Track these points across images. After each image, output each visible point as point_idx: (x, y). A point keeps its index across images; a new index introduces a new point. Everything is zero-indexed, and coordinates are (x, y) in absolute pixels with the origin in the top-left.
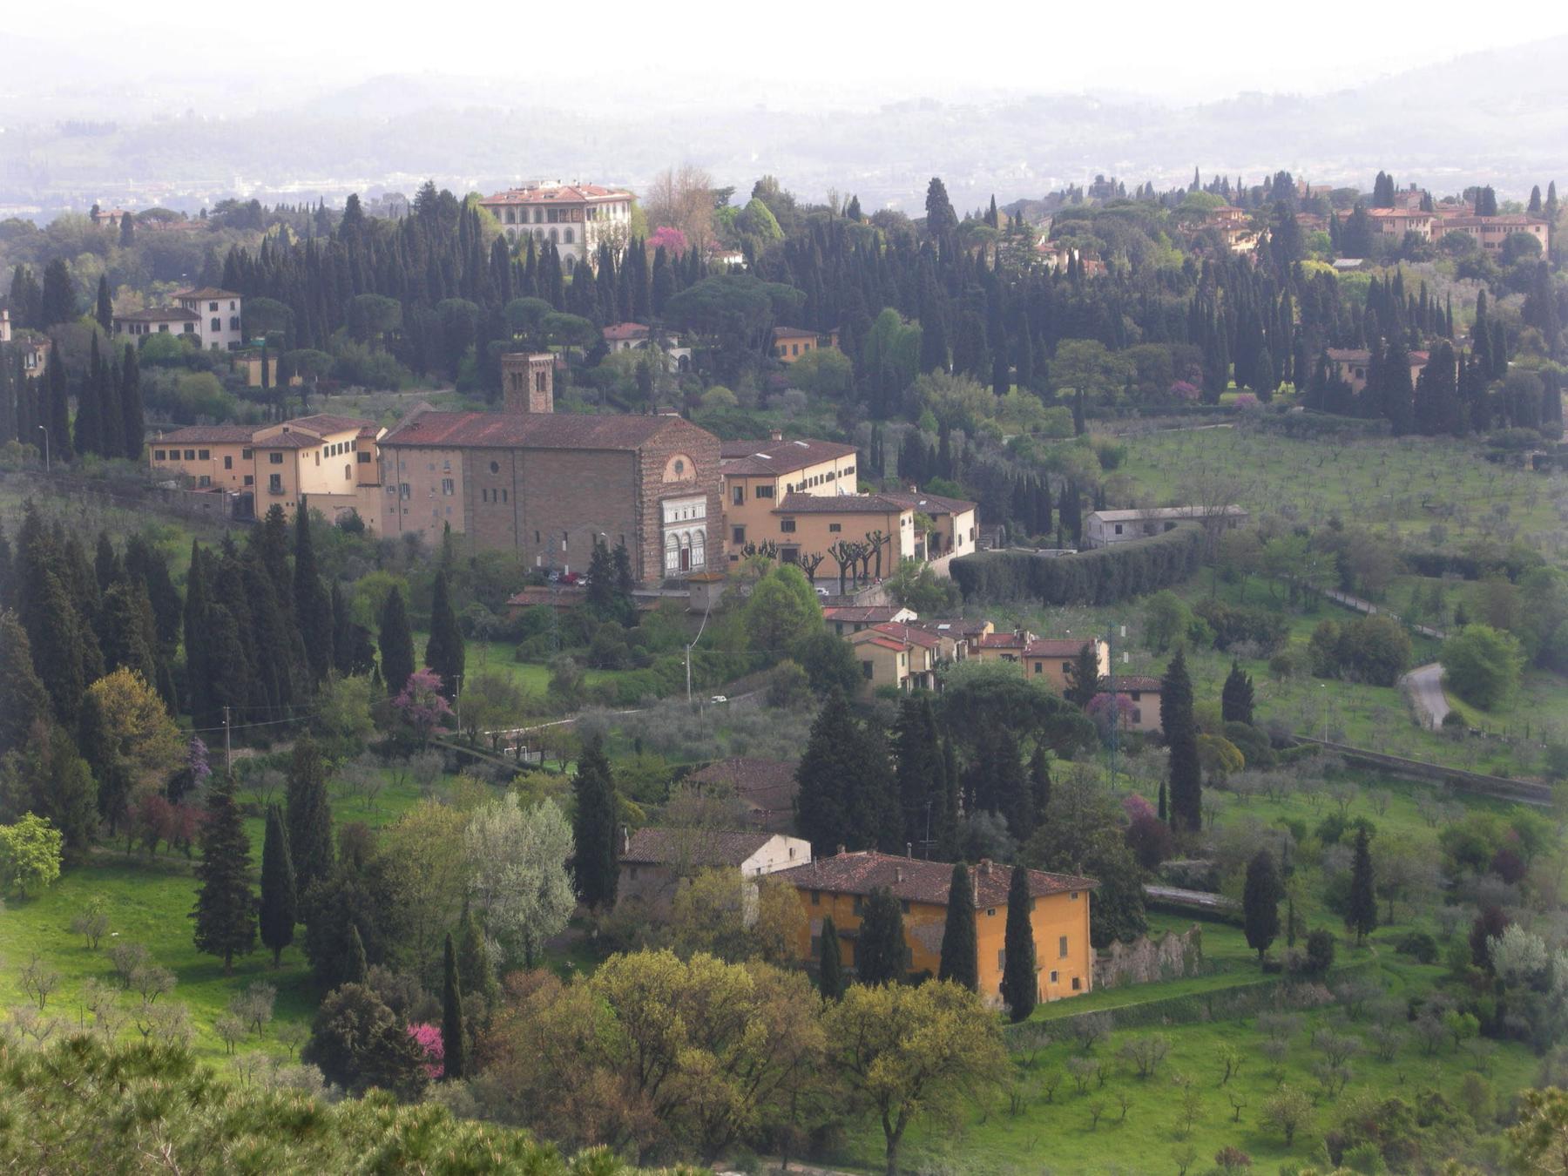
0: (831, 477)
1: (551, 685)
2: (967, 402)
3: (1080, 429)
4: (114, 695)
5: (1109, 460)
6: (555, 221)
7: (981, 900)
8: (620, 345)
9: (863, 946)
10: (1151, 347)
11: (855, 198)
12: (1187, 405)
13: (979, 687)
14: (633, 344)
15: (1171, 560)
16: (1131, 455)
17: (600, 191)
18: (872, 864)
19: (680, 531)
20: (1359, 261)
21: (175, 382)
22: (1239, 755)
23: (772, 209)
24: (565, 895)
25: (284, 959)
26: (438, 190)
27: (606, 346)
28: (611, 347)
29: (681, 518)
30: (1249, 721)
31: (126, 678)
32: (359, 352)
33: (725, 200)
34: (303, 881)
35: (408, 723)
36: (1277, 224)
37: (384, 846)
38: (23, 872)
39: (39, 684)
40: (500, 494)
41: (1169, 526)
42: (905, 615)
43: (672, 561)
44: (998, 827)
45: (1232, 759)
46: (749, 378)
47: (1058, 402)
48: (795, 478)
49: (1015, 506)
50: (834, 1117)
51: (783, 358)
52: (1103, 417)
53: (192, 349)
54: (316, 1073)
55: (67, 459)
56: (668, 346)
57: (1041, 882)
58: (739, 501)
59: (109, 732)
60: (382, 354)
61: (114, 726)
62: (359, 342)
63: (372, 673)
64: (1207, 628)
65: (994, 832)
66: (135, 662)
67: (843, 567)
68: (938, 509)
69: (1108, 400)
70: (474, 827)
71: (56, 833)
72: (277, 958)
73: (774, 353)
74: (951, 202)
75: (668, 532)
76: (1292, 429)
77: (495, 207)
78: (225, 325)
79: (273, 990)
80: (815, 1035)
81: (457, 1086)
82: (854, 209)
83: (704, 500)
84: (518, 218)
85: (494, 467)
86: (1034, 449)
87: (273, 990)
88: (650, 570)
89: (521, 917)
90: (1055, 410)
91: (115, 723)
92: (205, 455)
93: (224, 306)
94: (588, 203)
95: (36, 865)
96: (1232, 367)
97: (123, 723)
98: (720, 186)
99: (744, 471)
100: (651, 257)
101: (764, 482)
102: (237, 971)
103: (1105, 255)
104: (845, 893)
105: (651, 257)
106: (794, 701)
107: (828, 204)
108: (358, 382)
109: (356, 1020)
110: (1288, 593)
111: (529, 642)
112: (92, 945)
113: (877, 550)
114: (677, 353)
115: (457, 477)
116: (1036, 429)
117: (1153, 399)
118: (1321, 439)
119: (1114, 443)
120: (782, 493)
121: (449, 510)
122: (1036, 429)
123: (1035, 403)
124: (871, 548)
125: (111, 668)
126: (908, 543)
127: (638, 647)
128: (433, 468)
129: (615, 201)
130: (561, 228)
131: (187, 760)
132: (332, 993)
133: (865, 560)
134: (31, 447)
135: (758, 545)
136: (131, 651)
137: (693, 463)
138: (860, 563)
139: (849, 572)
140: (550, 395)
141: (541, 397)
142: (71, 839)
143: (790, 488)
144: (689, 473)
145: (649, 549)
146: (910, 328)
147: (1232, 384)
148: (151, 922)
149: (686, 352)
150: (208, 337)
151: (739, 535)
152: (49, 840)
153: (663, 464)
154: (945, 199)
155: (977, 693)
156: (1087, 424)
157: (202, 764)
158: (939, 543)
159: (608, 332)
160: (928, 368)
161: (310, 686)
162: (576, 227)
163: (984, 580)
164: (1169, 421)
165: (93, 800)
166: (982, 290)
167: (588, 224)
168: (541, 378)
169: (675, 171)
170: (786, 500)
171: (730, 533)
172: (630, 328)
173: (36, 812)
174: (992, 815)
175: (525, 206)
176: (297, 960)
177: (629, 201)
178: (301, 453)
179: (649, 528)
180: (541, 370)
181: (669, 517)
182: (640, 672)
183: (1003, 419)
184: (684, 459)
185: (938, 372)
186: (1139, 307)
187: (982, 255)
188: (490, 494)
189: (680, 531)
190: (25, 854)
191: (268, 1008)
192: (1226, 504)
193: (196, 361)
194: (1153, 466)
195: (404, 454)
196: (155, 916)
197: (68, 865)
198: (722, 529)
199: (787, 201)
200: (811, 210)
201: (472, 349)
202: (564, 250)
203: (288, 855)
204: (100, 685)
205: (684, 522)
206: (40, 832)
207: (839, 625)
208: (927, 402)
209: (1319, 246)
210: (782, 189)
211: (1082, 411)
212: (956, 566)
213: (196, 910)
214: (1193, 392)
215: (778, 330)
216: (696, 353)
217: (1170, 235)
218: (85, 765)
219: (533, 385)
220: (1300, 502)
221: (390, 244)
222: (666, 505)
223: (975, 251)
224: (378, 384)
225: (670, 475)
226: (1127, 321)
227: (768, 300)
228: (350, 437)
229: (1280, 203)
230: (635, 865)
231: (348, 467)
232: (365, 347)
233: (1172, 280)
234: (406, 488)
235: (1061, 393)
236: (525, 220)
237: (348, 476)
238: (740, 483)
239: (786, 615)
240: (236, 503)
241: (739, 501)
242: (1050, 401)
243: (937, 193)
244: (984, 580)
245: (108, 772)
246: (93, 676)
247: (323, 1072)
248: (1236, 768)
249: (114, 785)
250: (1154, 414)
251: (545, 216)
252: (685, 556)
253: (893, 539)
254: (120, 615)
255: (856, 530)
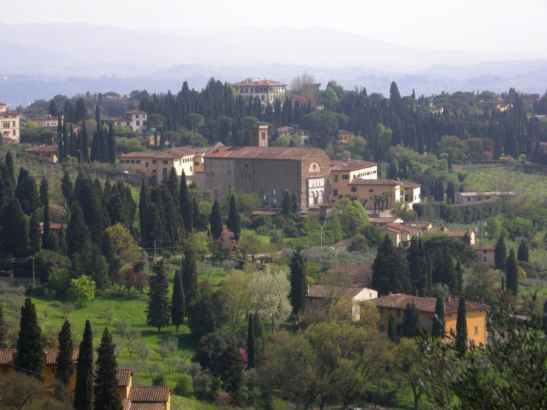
0: (368, 174)
1: (271, 240)
2: (409, 157)
3: (450, 167)
4: (115, 232)
5: (461, 178)
6: (258, 92)
7: (446, 311)
8: (283, 135)
9: (402, 325)
10: (475, 139)
11: (365, 88)
12: (488, 160)
13: (436, 240)
15: (490, 209)
16: (469, 177)
17: (274, 82)
18: (403, 298)
19: (314, 190)
20: (544, 116)
21: (124, 141)
22: (525, 273)
23: (335, 91)
24: (288, 307)
25: (179, 329)
26: (216, 80)
29: (315, 186)
30: (527, 261)
31: (119, 226)
33: (318, 88)
34: (188, 300)
35: (220, 250)
36: (515, 102)
38: (81, 296)
39: (87, 228)
40: (248, 176)
41: (488, 197)
42: (399, 221)
43: (311, 201)
44: (445, 289)
45: (522, 275)
46: (330, 146)
47: (442, 158)
48: (356, 173)
49: (432, 189)
50: (393, 389)
51: (341, 141)
52: (458, 163)
53: (129, 131)
54: (198, 365)
55: (88, 163)
56: (300, 135)
57: (468, 305)
58: (336, 180)
59: (112, 246)
61: (115, 244)
64: (506, 231)
65: (443, 291)
66: (122, 221)
67: (375, 204)
68: (408, 186)
69: (460, 158)
70: (254, 280)
71: (93, 282)
72: (177, 329)
73: (338, 139)
74: (399, 90)
75: (310, 190)
76: (527, 170)
77: (236, 86)
78: (141, 123)
79: (177, 339)
80: (390, 355)
81: (253, 370)
82: (364, 91)
83: (323, 179)
84: (244, 91)
85: (246, 166)
86: (434, 173)
87: (177, 339)
88: (303, 204)
89: (271, 314)
90: (441, 161)
91: (115, 243)
92: (138, 162)
93: (141, 116)
94: (270, 86)
95: (86, 294)
96: (503, 149)
97: (118, 243)
98: (317, 83)
99: (338, 169)
100: (293, 104)
101: (345, 174)
102: (163, 333)
103: (454, 110)
104: (394, 308)
105: (293, 104)
106: (361, 249)
107: (354, 90)
108: (191, 144)
109: (213, 346)
110: (531, 223)
111: (260, 228)
112: (107, 323)
113: (386, 199)
114: (304, 137)
115: (232, 169)
116: (434, 167)
117: (475, 157)
118: (538, 172)
119: (463, 172)
120: (351, 178)
121: (229, 182)
122: (434, 167)
123: (433, 157)
124: (385, 198)
125: (113, 223)
126: (398, 196)
128: (223, 166)
129: (279, 86)
130: (260, 95)
131: (140, 259)
132: (204, 337)
133: (383, 202)
134: (75, 158)
135: (344, 195)
136: (120, 218)
138: (381, 203)
139: (377, 205)
140: (267, 141)
141: (263, 141)
142: (99, 286)
143: (354, 176)
144: (318, 169)
145: (303, 196)
146: (387, 131)
147: (503, 154)
148: (129, 316)
150: (135, 128)
151: (335, 193)
152: (90, 285)
153: (309, 165)
154: (397, 89)
155: (435, 241)
156: (453, 166)
157: (146, 260)
158: (409, 198)
159: (279, 129)
160: (394, 145)
162: (265, 95)
163: (425, 211)
164: (482, 166)
165: (107, 270)
166: (412, 119)
167: (270, 94)
169: (301, 77)
170: (353, 180)
171: (332, 192)
172: (286, 128)
173: (85, 274)
174: (443, 285)
175: (247, 87)
176: (185, 329)
177: (284, 86)
179: (303, 189)
180: (263, 131)
181: (310, 185)
183: (424, 162)
184: (316, 164)
185: (398, 146)
186: (469, 126)
187: (412, 108)
189: (314, 190)
190: (81, 289)
191: (176, 345)
192: (508, 191)
193: (130, 135)
194: (477, 181)
195: (213, 161)
196: (130, 314)
197: (96, 295)
198: (330, 191)
199: (340, 88)
200: (348, 92)
201: (231, 133)
202: (263, 103)
203: (182, 289)
204: (109, 229)
205: (316, 187)
206: (87, 281)
207: (375, 224)
208: (395, 156)
209: (530, 111)
210: (338, 84)
211: (451, 162)
212: (415, 206)
213: (148, 310)
214: (490, 154)
215: (340, 131)
216: (310, 139)
217: (477, 104)
218: (103, 258)
219: (260, 136)
220: (532, 194)
221: (200, 97)
222: (310, 181)
223: (409, 107)
224: (197, 145)
225: (311, 170)
226: (466, 131)
227: (337, 119)
228: (192, 156)
229: (513, 97)
230: (311, 298)
231: (191, 167)
232: (192, 131)
233: (482, 118)
234: (213, 173)
235: (442, 155)
236: (247, 92)
237: (191, 170)
238: (337, 174)
239: (356, 219)
240: (150, 179)
241: (336, 180)
242: (439, 158)
243: (394, 88)
244: (425, 211)
245: (112, 261)
246: (106, 226)
247: (201, 365)
248: (524, 278)
249: (115, 265)
250: (476, 163)
251: (254, 91)
252: (316, 199)
253: (393, 195)
254: (117, 204)
255: (378, 192)
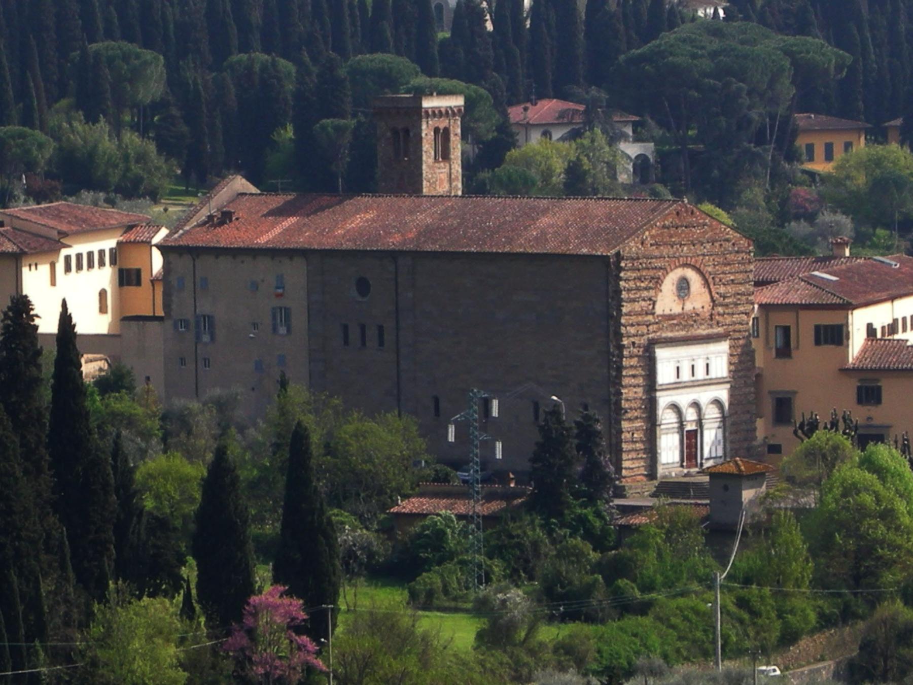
1: (480, 636)
8: (536, 137)
14: (557, 134)
19: (684, 399)
27: (512, 135)
28: (521, 138)
29: (686, 376)
32: (100, 138)
37: (865, 159)
40: (372, 333)
43: (669, 449)
46: (756, 192)
48: (879, 315)
56: (613, 140)
58: (784, 351)
60: (131, 138)
62: (91, 118)
63: (179, 598)
75: (663, 399)
83: (724, 347)
85: (363, 286)
88: (632, 464)
99: (794, 298)
101: (828, 319)
111: (431, 578)
114: (632, 150)
115: (297, 301)
120: (857, 342)
127: (622, 582)
128: (255, 286)
137: (706, 284)
140: (457, 168)
141: (442, 171)
144: (699, 299)
149: (647, 149)
151: (783, 408)
153: (657, 282)
159: (515, 113)
161: (75, 615)
168: (443, 136)
171: (768, 407)
172: (548, 108)
178: (25, 261)
179: (632, 392)
180: (443, 123)
181: (665, 374)
182: (631, 622)
184: (691, 274)
188: (354, 334)
189: (684, 399)
198: (756, 400)
215: (801, 119)
216: (662, 156)
222: (662, 354)
225: (667, 301)
227: (787, 63)
228: (109, 243)
231: (103, 294)
234: (207, 322)
237: (103, 309)
238: (787, 319)
241: (784, 351)
252: (690, 442)
